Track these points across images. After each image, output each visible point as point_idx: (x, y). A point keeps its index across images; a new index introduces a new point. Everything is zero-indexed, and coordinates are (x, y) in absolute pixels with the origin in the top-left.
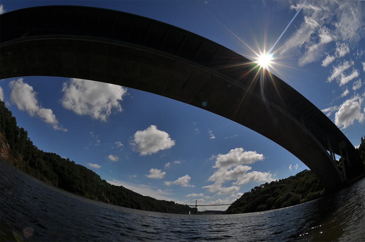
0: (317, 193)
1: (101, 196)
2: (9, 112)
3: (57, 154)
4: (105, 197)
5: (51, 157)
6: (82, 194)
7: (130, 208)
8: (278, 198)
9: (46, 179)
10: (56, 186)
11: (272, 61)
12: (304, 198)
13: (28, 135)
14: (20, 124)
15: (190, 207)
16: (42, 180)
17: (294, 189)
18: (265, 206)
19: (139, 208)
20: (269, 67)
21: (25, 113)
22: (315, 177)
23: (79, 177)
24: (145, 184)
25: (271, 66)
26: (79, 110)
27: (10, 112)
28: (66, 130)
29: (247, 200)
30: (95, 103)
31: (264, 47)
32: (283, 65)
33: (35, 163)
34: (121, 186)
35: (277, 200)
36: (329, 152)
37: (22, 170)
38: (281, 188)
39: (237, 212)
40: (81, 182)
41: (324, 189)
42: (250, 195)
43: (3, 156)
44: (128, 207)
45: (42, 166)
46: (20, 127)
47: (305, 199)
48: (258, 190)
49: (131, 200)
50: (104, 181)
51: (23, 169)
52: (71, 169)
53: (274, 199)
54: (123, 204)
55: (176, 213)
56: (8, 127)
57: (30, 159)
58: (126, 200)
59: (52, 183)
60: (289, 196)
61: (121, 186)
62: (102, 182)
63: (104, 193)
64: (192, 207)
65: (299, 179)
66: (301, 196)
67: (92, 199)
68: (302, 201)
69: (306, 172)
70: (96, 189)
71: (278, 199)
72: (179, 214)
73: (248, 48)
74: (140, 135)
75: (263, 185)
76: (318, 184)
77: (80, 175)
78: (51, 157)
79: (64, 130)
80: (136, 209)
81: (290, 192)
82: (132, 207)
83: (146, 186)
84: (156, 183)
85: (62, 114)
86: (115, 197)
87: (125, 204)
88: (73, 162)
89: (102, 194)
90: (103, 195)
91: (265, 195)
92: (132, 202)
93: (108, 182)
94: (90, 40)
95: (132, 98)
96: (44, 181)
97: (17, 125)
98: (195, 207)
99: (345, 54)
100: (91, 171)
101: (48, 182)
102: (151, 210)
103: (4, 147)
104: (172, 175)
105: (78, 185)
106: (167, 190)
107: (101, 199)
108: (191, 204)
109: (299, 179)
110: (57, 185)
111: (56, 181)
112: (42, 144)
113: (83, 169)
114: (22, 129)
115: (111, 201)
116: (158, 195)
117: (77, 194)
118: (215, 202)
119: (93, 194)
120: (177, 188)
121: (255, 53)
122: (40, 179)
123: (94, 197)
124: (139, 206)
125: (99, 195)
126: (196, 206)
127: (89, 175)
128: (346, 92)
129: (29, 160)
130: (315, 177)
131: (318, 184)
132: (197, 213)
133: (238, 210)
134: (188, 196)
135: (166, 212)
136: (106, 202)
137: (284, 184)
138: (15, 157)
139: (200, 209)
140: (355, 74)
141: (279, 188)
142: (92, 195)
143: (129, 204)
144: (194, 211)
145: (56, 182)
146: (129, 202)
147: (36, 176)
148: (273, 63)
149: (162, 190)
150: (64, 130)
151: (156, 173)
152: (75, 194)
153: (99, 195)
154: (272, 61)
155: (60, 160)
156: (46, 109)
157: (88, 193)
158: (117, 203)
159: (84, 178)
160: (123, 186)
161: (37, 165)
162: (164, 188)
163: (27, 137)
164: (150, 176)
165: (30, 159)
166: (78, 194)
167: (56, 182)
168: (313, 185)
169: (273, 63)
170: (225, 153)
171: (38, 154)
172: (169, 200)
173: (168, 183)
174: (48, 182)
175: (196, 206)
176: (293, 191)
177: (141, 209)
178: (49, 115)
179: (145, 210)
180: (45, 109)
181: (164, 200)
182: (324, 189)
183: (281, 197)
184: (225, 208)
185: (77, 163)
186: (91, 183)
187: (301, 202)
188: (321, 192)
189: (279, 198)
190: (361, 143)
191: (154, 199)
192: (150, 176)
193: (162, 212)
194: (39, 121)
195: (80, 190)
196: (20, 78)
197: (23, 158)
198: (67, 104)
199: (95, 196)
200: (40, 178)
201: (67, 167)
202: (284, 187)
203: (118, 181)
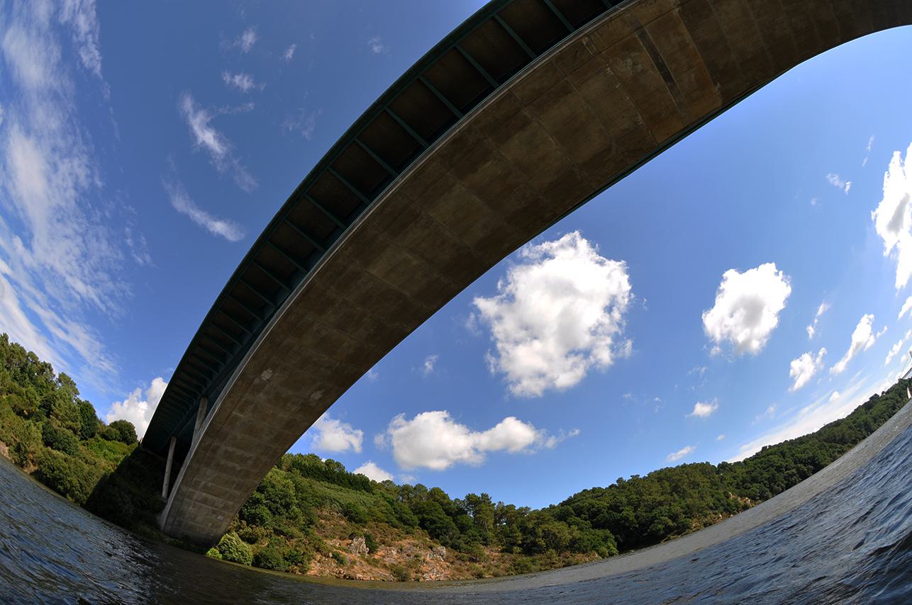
1: (729, 505)
4: (739, 499)
5: (576, 504)
6: (681, 530)
9: (579, 556)
10: (611, 555)
14: (456, 493)
16: (568, 565)
19: (818, 467)
21: (459, 468)
23: (662, 498)
24: (806, 406)
26: (566, 378)
28: (577, 432)
30: (585, 340)
33: (537, 540)
34: (764, 448)
37: (504, 575)
40: (670, 505)
43: (433, 577)
45: (559, 535)
46: (462, 498)
49: (795, 463)
50: (724, 466)
51: (507, 571)
52: (634, 496)
54: (782, 485)
56: (424, 515)
58: (786, 470)
59: (600, 555)
61: (763, 448)
62: (718, 473)
63: (733, 492)
67: (710, 525)
70: (713, 496)
74: (716, 320)
77: (662, 494)
78: (576, 504)
79: (571, 434)
82: (804, 476)
84: (820, 385)
85: (544, 409)
86: (760, 483)
87: (786, 482)
88: (635, 478)
89: (728, 497)
90: (732, 497)
92: (799, 465)
93: (731, 461)
97: (452, 498)
100: (684, 466)
103: (428, 559)
104: (837, 342)
105: (667, 518)
106: (852, 380)
107: (730, 510)
110: (615, 550)
111: (609, 544)
112: (539, 496)
113: (662, 477)
115: (753, 499)
116: (840, 407)
118: (484, 439)
119: (708, 512)
120: (864, 360)
122: (564, 566)
123: (714, 516)
124: (817, 462)
125: (723, 505)
127: (675, 481)
129: (519, 545)
134: (888, 360)
136: (746, 508)
138: (472, 560)
142: (705, 516)
143: (795, 475)
145: (608, 548)
146: (794, 471)
147: (552, 565)
149: (840, 391)
150: (571, 434)
151: (803, 368)
153: (723, 505)
155: (602, 495)
156: (494, 427)
157: (695, 520)
158: (769, 493)
159: (674, 493)
160: (767, 445)
161: (542, 542)
162: (840, 383)
163: (493, 503)
164: (799, 383)
166: (672, 537)
167: (608, 548)
171: (538, 519)
172: (865, 399)
173: (840, 366)
174: (587, 559)
178: (515, 431)
180: (494, 429)
185: (643, 474)
186: (695, 493)
191: (838, 423)
192: (799, 383)
194: (500, 460)
195: (675, 524)
196: (705, 331)
198: (532, 387)
199: (716, 514)
200: (564, 564)
201: (624, 498)
203: (751, 443)
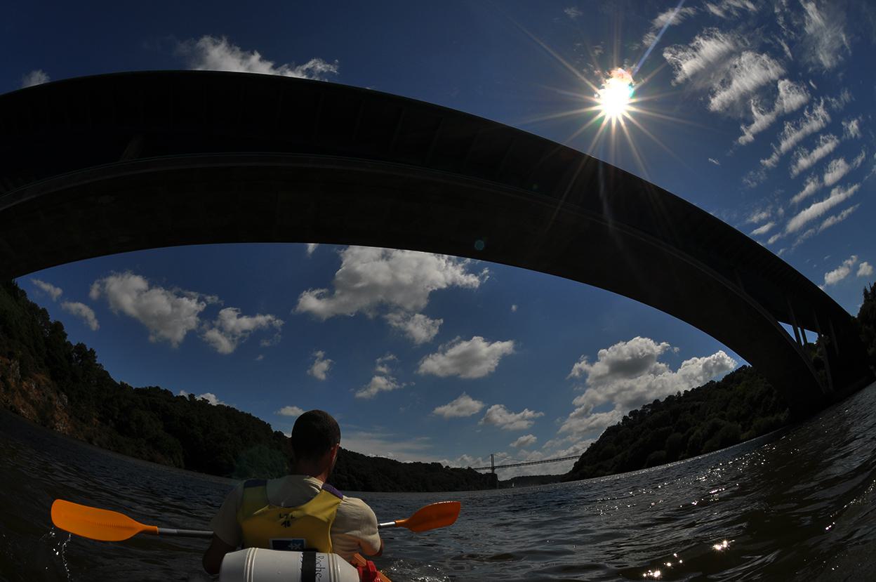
2: (40, 311)
3: (163, 388)
8: (691, 433)
10: (180, 467)
11: (633, 104)
12: (747, 431)
13: (97, 359)
16: (152, 460)
17: (724, 412)
18: (663, 453)
20: (625, 119)
22: (766, 383)
25: (629, 116)
27: (44, 310)
31: (646, 110)
32: (659, 116)
36: (789, 329)
39: (600, 472)
41: (788, 409)
42: (621, 432)
46: (74, 344)
47: (750, 431)
48: (637, 418)
53: (682, 436)
57: (116, 417)
60: (716, 427)
64: (483, 472)
65: (731, 389)
66: (740, 426)
68: (743, 436)
69: (745, 373)
71: (692, 436)
73: (576, 76)
76: (774, 399)
80: (363, 491)
81: (715, 419)
83: (370, 434)
91: (660, 430)
96: (158, 463)
98: (489, 471)
101: (166, 462)
102: (394, 490)
108: (482, 465)
109: (731, 389)
114: (81, 347)
121: (591, 88)
126: (493, 468)
128: (810, 188)
130: (766, 383)
131: (774, 399)
132: (498, 484)
135: (428, 491)
137: (699, 402)
139: (503, 476)
140: (828, 147)
144: (490, 481)
148: (633, 109)
154: (633, 104)
165: (116, 417)
169: (633, 109)
172: (427, 460)
176: (723, 417)
179: (383, 491)
181: (418, 461)
182: (788, 409)
183: (698, 431)
184: (568, 466)
185: (423, 462)
187: (741, 438)
189: (695, 434)
191: (394, 463)
193: (419, 491)
197: (98, 419)
202: (699, 407)
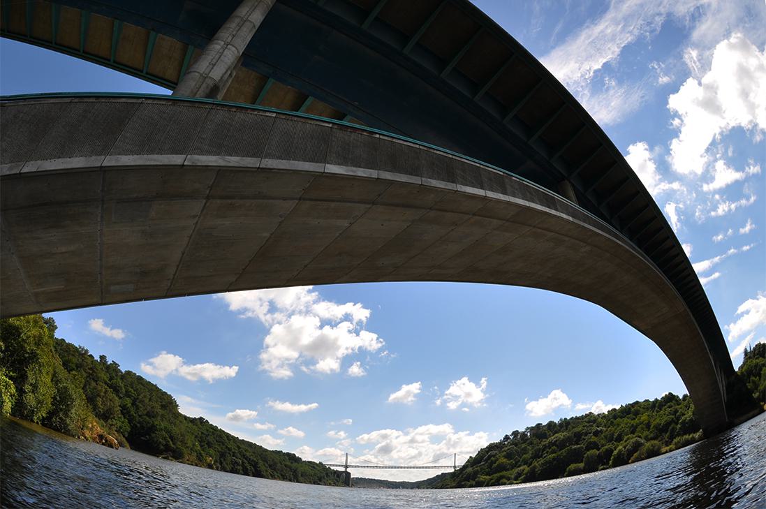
0: (691, 436)
7: (241, 474)
15: (332, 468)
18: (581, 465)
29: (509, 456)
35: (615, 452)
38: (596, 434)
44: (238, 473)
55: (314, 483)
72: (319, 484)
75: (532, 429)
76: (679, 426)
80: (253, 476)
83: (193, 401)
94: (638, 255)
95: (730, 231)
99: (729, 183)
117: (168, 459)
131: (679, 426)
133: (163, 395)
141: (590, 433)
152: (163, 458)
166: (170, 458)
168: (670, 428)
170: (437, 424)
175: (346, 467)
177: (262, 476)
182: (701, 430)
188: (697, 435)
190: (659, 399)
193: (290, 481)
202: (601, 431)
